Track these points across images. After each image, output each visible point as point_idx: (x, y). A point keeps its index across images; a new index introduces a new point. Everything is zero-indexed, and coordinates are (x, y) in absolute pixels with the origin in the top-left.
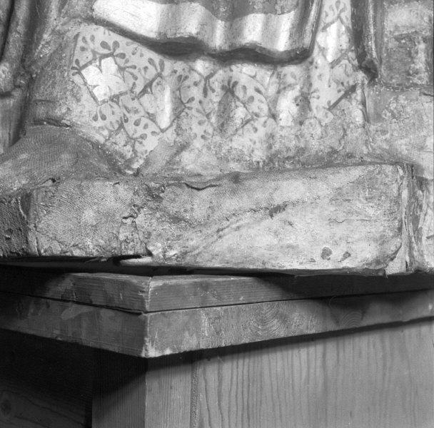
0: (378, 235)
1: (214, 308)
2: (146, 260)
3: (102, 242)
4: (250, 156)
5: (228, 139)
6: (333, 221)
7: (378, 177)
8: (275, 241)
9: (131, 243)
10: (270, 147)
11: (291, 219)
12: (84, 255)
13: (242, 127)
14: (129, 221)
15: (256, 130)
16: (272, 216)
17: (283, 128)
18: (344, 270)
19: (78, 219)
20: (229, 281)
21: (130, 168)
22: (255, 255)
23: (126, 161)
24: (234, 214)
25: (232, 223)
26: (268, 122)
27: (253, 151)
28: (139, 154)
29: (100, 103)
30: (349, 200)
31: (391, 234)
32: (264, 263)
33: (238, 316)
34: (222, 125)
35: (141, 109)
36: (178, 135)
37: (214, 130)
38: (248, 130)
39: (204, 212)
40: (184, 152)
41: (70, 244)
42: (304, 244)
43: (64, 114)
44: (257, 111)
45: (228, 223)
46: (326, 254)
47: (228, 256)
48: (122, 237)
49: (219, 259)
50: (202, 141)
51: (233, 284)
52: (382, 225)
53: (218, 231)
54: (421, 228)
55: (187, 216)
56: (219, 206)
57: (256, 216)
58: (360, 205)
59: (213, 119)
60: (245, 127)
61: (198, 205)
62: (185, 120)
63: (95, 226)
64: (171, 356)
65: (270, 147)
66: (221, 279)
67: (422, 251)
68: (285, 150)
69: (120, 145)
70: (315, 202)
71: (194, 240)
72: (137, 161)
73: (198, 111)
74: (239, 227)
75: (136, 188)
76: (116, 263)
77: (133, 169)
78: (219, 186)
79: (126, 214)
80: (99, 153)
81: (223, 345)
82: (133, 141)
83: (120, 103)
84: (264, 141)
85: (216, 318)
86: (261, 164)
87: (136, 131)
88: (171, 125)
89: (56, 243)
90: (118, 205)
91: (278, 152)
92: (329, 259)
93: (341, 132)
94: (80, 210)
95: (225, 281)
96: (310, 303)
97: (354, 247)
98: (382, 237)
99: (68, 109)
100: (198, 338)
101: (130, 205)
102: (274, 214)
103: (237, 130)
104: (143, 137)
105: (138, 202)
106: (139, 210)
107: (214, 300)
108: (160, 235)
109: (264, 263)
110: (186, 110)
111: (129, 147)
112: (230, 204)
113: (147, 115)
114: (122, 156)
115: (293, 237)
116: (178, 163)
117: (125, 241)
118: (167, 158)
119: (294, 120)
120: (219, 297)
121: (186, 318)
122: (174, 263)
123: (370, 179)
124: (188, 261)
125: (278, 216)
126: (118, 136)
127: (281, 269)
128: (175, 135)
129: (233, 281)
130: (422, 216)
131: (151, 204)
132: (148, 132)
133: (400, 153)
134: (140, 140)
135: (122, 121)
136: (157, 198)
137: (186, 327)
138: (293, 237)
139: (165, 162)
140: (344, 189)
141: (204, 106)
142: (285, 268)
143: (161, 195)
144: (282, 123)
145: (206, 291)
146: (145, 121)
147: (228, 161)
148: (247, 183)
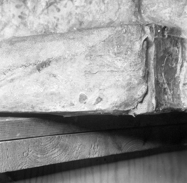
0: (124, 84)
4: (54, 29)
6: (88, 73)
7: (125, 35)
11: (55, 72)
13: (47, 8)
16: (39, 70)
18: (98, 112)
20: (3, 122)
22: (25, 101)
24: (9, 70)
25: (8, 77)
26: (68, 5)
27: (57, 26)
30: (101, 56)
31: (136, 82)
38: (53, 11)
40: (6, 28)
42: (64, 91)
45: (5, 76)
46: (83, 98)
50: (20, 20)
51: (8, 124)
52: (128, 75)
54: (179, 77)
57: (26, 71)
58: (109, 59)
60: (50, 8)
67: (179, 95)
70: (73, 58)
74: (12, 80)
92: (85, 103)
93: (117, 7)
96: (91, 135)
97: (105, 93)
98: (128, 84)
109: (33, 107)
115: (56, 86)
123: (118, 38)
125: (45, 70)
127: (47, 111)
130: (179, 68)
133: (164, 20)
138: (56, 86)
140: (97, 47)
142: (50, 111)
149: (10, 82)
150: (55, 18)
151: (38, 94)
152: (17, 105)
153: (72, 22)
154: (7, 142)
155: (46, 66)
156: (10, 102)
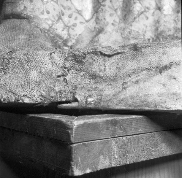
1: (121, 138)
2: (74, 105)
3: (44, 93)
4: (144, 35)
5: (129, 25)
8: (164, 90)
9: (64, 93)
10: (157, 29)
12: (32, 102)
13: (139, 16)
14: (61, 79)
15: (147, 18)
16: (161, 73)
17: (165, 15)
19: (27, 77)
20: (131, 119)
21: (66, 45)
23: (64, 41)
24: (134, 73)
26: (155, 13)
27: (145, 32)
28: (72, 36)
29: (45, 3)
32: (178, 12)
33: (138, 142)
34: (125, 16)
35: (72, 7)
36: (97, 23)
37: (120, 19)
38: (143, 18)
39: (113, 71)
41: (21, 94)
43: (22, 11)
44: (148, 5)
45: (130, 78)
47: (130, 102)
48: (57, 89)
49: (124, 103)
50: (112, 27)
53: (123, 84)
55: (101, 74)
56: (124, 67)
57: (149, 73)
59: (119, 12)
60: (141, 16)
61: (109, 68)
62: (101, 14)
63: (39, 82)
64: (91, 173)
65: (157, 29)
66: (126, 117)
68: (167, 30)
69: (60, 29)
71: (108, 91)
72: (71, 41)
73: (110, 7)
74: (137, 82)
75: (66, 55)
76: (54, 107)
77: (68, 46)
78: (124, 53)
79: (59, 74)
80: (45, 35)
81: (128, 163)
82: (68, 28)
83: (59, 3)
84: (153, 25)
85: (122, 145)
86: (151, 41)
87: (69, 22)
88: (92, 18)
89: (11, 94)
90: (54, 68)
91: (163, 32)
94: (27, 71)
95: (128, 119)
99: (25, 7)
100: (110, 159)
101: (62, 67)
102: (163, 72)
103: (135, 18)
104: (75, 25)
105: (67, 65)
106: (68, 71)
107: (120, 132)
108: (83, 87)
109: (156, 106)
110: (102, 7)
111: (65, 32)
112: (131, 65)
113: (77, 11)
114: (61, 38)
116: (97, 41)
117: (60, 92)
118: (90, 39)
119: (173, 10)
120: (125, 130)
121: (101, 146)
122: (92, 106)
124: (102, 105)
126: (57, 25)
128: (95, 24)
129: (134, 118)
131: (78, 67)
132: (77, 22)
134: (72, 27)
135: (60, 15)
136: (81, 63)
137: (101, 152)
139: (89, 41)
141: (113, 3)
142: (171, 109)
143: (83, 60)
144: (165, 13)
145: (115, 126)
146: (75, 15)
147: (129, 39)
148: (143, 50)
149: (135, 83)
150: (144, 25)
151: (161, 94)
152: (142, 103)
153: (160, 29)
154: (133, 136)
155: (167, 69)
156: (136, 101)
